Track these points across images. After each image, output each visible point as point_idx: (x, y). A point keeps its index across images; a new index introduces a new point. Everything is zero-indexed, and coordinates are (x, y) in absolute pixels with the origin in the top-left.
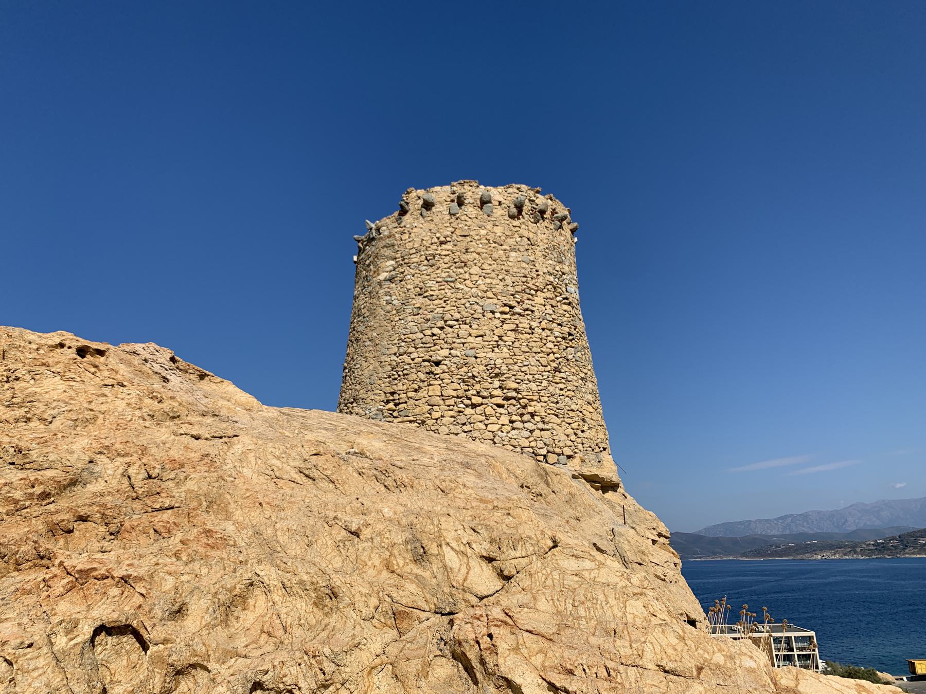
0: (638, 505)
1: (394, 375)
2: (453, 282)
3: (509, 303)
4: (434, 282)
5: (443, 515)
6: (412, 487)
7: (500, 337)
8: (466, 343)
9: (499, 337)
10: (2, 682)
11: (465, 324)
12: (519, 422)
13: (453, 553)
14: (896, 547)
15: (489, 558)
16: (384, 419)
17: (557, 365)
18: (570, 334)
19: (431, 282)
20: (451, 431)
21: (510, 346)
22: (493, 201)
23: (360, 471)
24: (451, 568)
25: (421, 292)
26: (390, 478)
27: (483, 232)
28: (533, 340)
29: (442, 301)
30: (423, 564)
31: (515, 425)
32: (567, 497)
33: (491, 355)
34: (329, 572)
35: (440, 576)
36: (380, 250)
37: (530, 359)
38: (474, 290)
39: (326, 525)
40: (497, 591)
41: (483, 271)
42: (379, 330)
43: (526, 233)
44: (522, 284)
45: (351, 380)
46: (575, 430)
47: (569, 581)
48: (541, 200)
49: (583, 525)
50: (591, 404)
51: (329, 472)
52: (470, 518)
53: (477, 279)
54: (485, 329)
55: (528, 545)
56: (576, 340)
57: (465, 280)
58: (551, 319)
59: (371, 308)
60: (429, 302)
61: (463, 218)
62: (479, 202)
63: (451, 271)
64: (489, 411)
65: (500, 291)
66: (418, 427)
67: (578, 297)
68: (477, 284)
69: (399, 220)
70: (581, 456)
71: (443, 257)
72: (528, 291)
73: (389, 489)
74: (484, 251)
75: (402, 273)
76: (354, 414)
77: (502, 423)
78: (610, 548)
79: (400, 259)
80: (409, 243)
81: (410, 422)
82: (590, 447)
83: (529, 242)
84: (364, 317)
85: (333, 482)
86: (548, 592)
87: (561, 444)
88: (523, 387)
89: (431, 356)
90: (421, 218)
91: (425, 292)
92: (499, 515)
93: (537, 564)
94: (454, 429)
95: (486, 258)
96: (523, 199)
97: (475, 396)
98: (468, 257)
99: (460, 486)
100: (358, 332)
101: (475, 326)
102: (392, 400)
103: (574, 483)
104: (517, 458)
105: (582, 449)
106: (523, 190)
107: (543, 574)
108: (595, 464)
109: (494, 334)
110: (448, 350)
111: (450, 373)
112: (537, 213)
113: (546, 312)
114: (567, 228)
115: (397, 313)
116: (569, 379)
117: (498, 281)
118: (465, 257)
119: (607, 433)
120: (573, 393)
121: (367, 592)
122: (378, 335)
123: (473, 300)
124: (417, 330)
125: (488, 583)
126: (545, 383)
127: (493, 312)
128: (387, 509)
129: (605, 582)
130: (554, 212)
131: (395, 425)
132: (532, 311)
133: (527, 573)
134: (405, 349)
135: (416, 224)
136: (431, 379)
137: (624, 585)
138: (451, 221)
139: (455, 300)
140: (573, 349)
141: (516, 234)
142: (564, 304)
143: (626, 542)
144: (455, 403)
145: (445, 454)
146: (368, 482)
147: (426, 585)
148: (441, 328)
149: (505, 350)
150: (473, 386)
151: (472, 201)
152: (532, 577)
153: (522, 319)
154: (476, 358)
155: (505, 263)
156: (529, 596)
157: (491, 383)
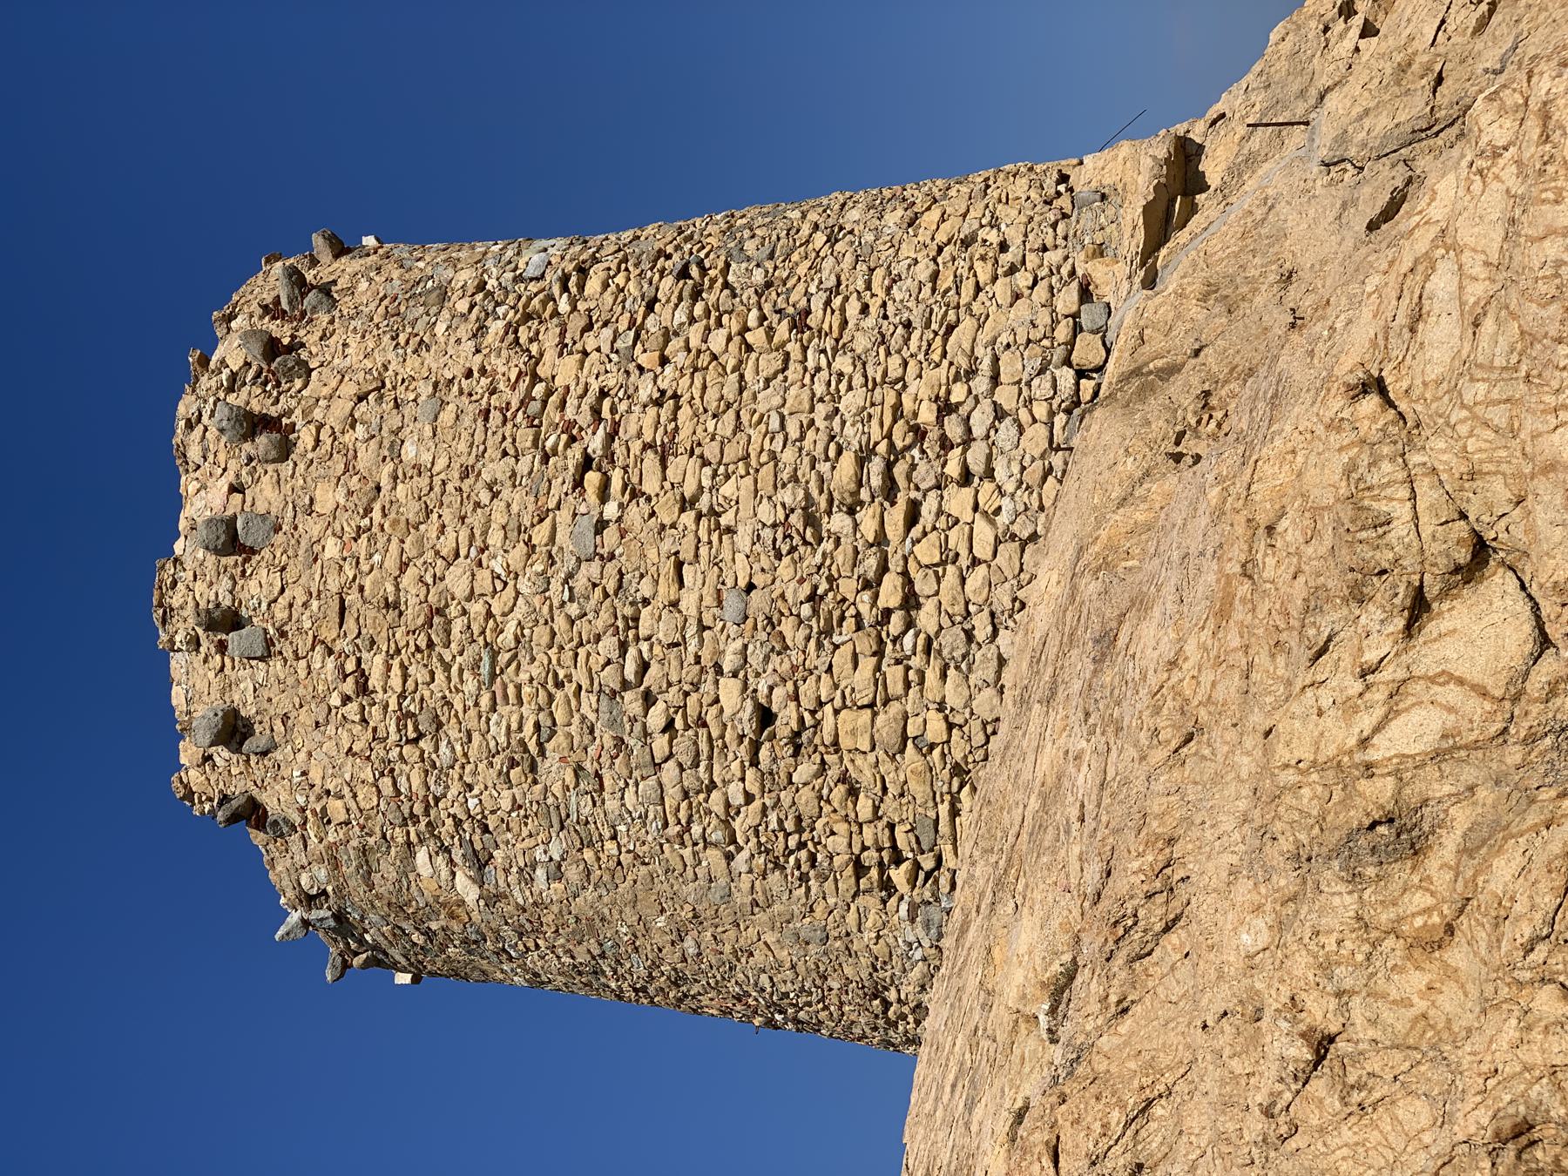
0: (1250, 77)
1: (798, 861)
2: (494, 656)
3: (572, 470)
4: (494, 717)
5: (1267, 752)
6: (1171, 841)
7: (685, 504)
8: (700, 621)
9: (682, 510)
10: (1566, 941)
11: (636, 619)
12: (969, 455)
13: (1395, 727)
15: (1412, 608)
17: (785, 322)
18: (684, 274)
20: (991, 678)
21: (715, 471)
22: (229, 513)
23: (1113, 1009)
24: (1443, 736)
25: (526, 764)
26: (1141, 913)
27: (332, 549)
28: (697, 396)
30: (1426, 828)
31: (977, 467)
32: (1216, 310)
33: (743, 539)
34: (1443, 1145)
35: (1469, 774)
37: (761, 408)
38: (524, 586)
39: (1292, 1144)
40: (1523, 587)
41: (463, 552)
42: (647, 908)
43: (341, 407)
44: (509, 425)
45: (809, 1004)
46: (1000, 271)
47: (1498, 351)
48: (232, 352)
49: (1307, 261)
50: (916, 216)
51: (1116, 1116)
52: (1281, 660)
53: (486, 574)
54: (657, 555)
55: (1374, 478)
56: (702, 255)
57: (489, 615)
58: (632, 333)
59: (573, 932)
60: (560, 739)
62: (230, 560)
64: (927, 552)
65: (532, 499)
66: (974, 789)
67: (561, 242)
68: (503, 575)
69: (280, 830)
70: (1082, 256)
71: (410, 685)
72: (534, 407)
73: (1177, 919)
74: (394, 546)
75: (458, 823)
76: (925, 998)
77: (969, 510)
78: (1387, 177)
79: (412, 830)
80: (360, 797)
81: (954, 813)
82: (1054, 226)
84: (603, 956)
85: (1149, 1103)
86: (1530, 424)
87: (1044, 318)
90: (277, 755)
91: (526, 750)
92: (1270, 561)
93: (1438, 451)
94: (983, 671)
95: (420, 542)
96: (226, 410)
97: (876, 597)
98: (412, 601)
99: (1174, 680)
101: (646, 589)
102: (881, 873)
103: (1170, 283)
104: (1083, 465)
106: (194, 409)
107: (1471, 435)
108: (1110, 211)
109: (673, 526)
110: (722, 681)
111: (798, 675)
112: (273, 366)
113: (606, 349)
114: (329, 269)
115: (591, 844)
116: (832, 282)
117: (499, 505)
118: (414, 614)
119: (1008, 167)
120: (879, 274)
121: (1514, 1022)
122: (663, 911)
123: (556, 590)
124: (652, 781)
125: (1495, 617)
126: (843, 363)
127: (601, 526)
128: (1245, 937)
129: (1503, 234)
130: (272, 310)
131: (965, 868)
132: (603, 394)
133: (1467, 485)
134: (714, 822)
135: (297, 773)
136: (817, 740)
137: (1514, 169)
138: (288, 653)
139: (555, 650)
140: (734, 266)
142: (581, 287)
143: (1367, 122)
144: (898, 662)
145: (1067, 711)
146: (1150, 984)
147: (1497, 822)
148: (649, 700)
149: (728, 489)
150: (844, 600)
151: (226, 583)
152: (1480, 473)
153: (629, 428)
154: (751, 587)
155: (437, 481)
156: (1541, 485)
157: (838, 542)
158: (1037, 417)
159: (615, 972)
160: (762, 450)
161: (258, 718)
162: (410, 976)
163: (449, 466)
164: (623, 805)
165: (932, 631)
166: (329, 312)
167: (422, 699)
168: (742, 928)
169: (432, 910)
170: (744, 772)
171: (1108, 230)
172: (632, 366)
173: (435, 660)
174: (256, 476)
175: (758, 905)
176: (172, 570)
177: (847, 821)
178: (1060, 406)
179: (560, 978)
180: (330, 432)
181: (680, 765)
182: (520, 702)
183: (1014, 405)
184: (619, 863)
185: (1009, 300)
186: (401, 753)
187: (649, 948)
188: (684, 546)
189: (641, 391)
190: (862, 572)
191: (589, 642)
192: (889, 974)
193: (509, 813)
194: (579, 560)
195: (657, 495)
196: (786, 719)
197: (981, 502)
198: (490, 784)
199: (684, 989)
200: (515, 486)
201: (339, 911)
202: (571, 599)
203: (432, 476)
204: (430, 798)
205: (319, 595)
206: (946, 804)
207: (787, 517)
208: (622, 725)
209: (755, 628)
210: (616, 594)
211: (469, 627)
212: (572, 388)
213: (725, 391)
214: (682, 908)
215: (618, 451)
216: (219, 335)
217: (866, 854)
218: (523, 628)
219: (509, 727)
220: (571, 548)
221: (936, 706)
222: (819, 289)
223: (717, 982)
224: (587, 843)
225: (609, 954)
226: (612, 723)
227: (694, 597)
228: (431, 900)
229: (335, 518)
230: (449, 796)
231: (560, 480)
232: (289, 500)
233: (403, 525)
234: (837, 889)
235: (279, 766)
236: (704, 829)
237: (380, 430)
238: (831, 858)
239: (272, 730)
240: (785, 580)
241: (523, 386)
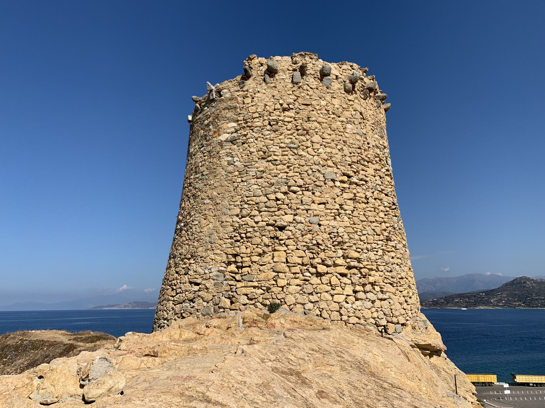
1: (237, 236)
2: (296, 148)
3: (348, 172)
4: (278, 148)
8: (309, 210)
9: (339, 205)
11: (307, 190)
12: (361, 293)
14: (443, 303)
16: (226, 282)
19: (275, 147)
20: (298, 301)
25: (264, 156)
27: (323, 103)
29: (285, 167)
33: (333, 223)
36: (220, 111)
37: (367, 228)
38: (316, 158)
41: (324, 140)
42: (219, 190)
43: (359, 108)
53: (319, 147)
54: (327, 197)
57: (307, 147)
58: (380, 190)
59: (210, 167)
60: (273, 167)
61: (305, 87)
62: (319, 74)
63: (294, 138)
64: (334, 281)
65: (340, 161)
69: (241, 84)
70: (412, 323)
71: (286, 123)
72: (362, 162)
74: (325, 121)
75: (245, 135)
77: (346, 294)
79: (242, 122)
80: (252, 107)
81: (255, 287)
83: (361, 116)
88: (363, 256)
89: (276, 221)
90: (264, 84)
91: (269, 156)
95: (326, 128)
97: (320, 264)
100: (196, 188)
101: (317, 194)
105: (411, 316)
110: (292, 216)
113: (377, 182)
115: (240, 174)
117: (337, 151)
118: (307, 125)
120: (399, 261)
122: (219, 194)
123: (315, 167)
124: (261, 194)
127: (333, 181)
132: (366, 181)
134: (249, 212)
135: (259, 90)
138: (294, 89)
139: (298, 166)
141: (351, 107)
148: (285, 193)
149: (346, 218)
150: (318, 254)
151: (313, 72)
153: (359, 189)
160: (357, 229)
161: (275, 79)
163: (346, 137)
164: (253, 185)
165: (312, 282)
166: (377, 106)
167: (282, 127)
168: (214, 217)
170: (265, 221)
171: (419, 330)
172: (374, 190)
173: (294, 131)
174: (340, 83)
175: (222, 223)
176: (315, 58)
177: (251, 253)
178: (377, 321)
179: (194, 162)
180: (353, 104)
181: (266, 202)
182: (283, 155)
184: (234, 182)
185: (400, 302)
186: (266, 120)
188: (330, 205)
190: (327, 260)
191: (301, 176)
192: (200, 261)
193: (249, 151)
195: (343, 197)
196: (282, 235)
198: (258, 145)
199: (192, 198)
200: (342, 156)
201: (215, 100)
202: (313, 172)
203: (343, 132)
205: (310, 98)
206: (257, 285)
207: (340, 236)
208: (278, 185)
210: (315, 185)
211: (303, 141)
213: (370, 217)
214: (220, 200)
217: (240, 258)
218: (304, 157)
219: (275, 152)
220: (327, 172)
221: (289, 283)
222: (396, 244)
223: (195, 208)
225: (204, 177)
226: (278, 183)
228: (220, 126)
229: (331, 104)
230: (253, 133)
231: (345, 169)
232: (335, 92)
234: (228, 248)
235: (260, 85)
236: (246, 208)
237: (354, 118)
238: (238, 247)
239: (271, 83)
240: (323, 236)
241: (367, 159)
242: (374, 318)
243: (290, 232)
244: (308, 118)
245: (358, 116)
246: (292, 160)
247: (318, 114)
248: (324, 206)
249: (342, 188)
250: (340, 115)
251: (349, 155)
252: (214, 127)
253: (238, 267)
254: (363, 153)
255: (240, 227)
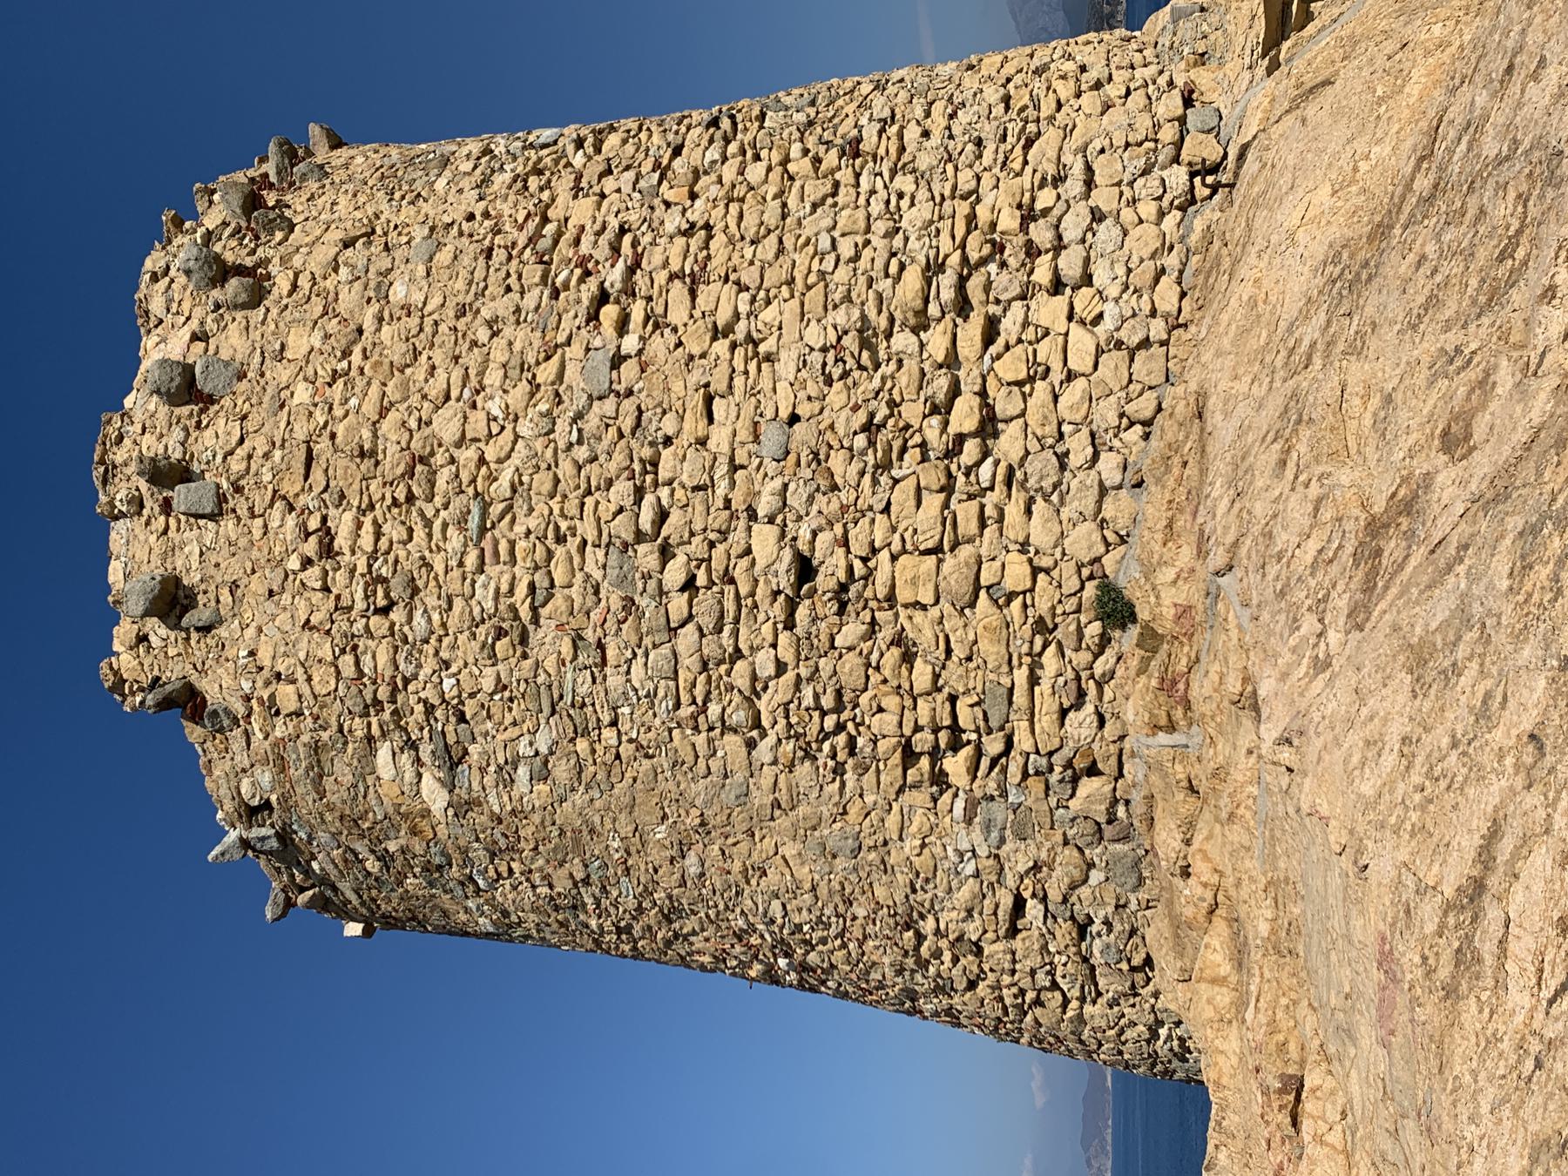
1: (833, 748)
3: (586, 302)
4: (481, 579)
8: (732, 459)
9: (714, 339)
11: (655, 465)
12: (1061, 263)
16: (1012, 791)
25: (515, 635)
27: (302, 393)
29: (560, 551)
33: (786, 366)
36: (330, 808)
37: (807, 232)
38: (524, 428)
41: (454, 394)
43: (325, 253)
44: (515, 262)
45: (823, 941)
46: (1084, 87)
53: (481, 415)
54: (685, 388)
57: (482, 461)
58: (657, 175)
59: (555, 850)
60: (558, 601)
62: (185, 410)
63: (443, 513)
64: (1012, 367)
65: (538, 334)
69: (219, 722)
70: (1183, 65)
71: (383, 544)
72: (544, 244)
74: (374, 390)
75: (429, 709)
77: (1065, 321)
79: (374, 720)
80: (316, 679)
81: (1034, 681)
83: (359, 244)
84: (586, 881)
88: (918, 249)
90: (222, 632)
91: (517, 617)
97: (946, 423)
98: (392, 449)
100: (640, 909)
101: (669, 425)
105: (1153, 69)
106: (162, 263)
110: (755, 527)
111: (849, 517)
113: (626, 189)
115: (586, 733)
118: (392, 461)
122: (664, 817)
124: (665, 650)
127: (617, 361)
132: (623, 231)
134: (737, 699)
135: (243, 653)
138: (243, 511)
139: (558, 498)
140: (770, 114)
144: (971, 497)
148: (666, 553)
149: (769, 315)
150: (907, 427)
151: (177, 434)
153: (653, 259)
154: (794, 419)
155: (428, 321)
158: (1143, 217)
159: (598, 905)
160: (810, 271)
161: (203, 587)
162: (361, 926)
164: (628, 681)
165: (1015, 457)
167: (396, 561)
169: (390, 824)
170: (776, 636)
171: (1212, 37)
175: (779, 807)
179: (532, 916)
181: (700, 629)
183: (1115, 205)
184: (618, 756)
186: (367, 626)
187: (643, 868)
189: (667, 224)
190: (930, 392)
191: (598, 489)
192: (929, 895)
193: (492, 694)
194: (590, 397)
197: (1077, 309)
198: (471, 660)
199: (676, 925)
200: (518, 323)
201: (283, 829)
202: (580, 442)
204: (399, 681)
205: (283, 446)
206: (1025, 669)
207: (839, 339)
209: (798, 464)
210: (633, 434)
211: (457, 476)
212: (587, 228)
213: (765, 217)
214: (687, 813)
215: (640, 282)
216: (200, 209)
217: (918, 736)
219: (497, 590)
220: (582, 385)
221: (1018, 547)
223: (718, 914)
224: (581, 731)
225: (594, 877)
226: (622, 581)
227: (728, 430)
228: (391, 810)
231: (572, 313)
232: (257, 345)
233: (386, 367)
234: (879, 783)
236: (724, 709)
239: (218, 601)
240: (836, 407)
241: (531, 226)
242: (1161, 214)
243: (820, 536)
244: (362, 455)
245: (357, 254)
246: (532, 523)
247: (346, 416)
248: (717, 400)
249: (650, 327)
250: (353, 326)
251: (515, 296)
252: (392, 835)
253: (955, 746)
254: (510, 237)
255: (797, 736)
